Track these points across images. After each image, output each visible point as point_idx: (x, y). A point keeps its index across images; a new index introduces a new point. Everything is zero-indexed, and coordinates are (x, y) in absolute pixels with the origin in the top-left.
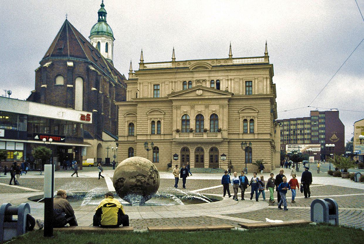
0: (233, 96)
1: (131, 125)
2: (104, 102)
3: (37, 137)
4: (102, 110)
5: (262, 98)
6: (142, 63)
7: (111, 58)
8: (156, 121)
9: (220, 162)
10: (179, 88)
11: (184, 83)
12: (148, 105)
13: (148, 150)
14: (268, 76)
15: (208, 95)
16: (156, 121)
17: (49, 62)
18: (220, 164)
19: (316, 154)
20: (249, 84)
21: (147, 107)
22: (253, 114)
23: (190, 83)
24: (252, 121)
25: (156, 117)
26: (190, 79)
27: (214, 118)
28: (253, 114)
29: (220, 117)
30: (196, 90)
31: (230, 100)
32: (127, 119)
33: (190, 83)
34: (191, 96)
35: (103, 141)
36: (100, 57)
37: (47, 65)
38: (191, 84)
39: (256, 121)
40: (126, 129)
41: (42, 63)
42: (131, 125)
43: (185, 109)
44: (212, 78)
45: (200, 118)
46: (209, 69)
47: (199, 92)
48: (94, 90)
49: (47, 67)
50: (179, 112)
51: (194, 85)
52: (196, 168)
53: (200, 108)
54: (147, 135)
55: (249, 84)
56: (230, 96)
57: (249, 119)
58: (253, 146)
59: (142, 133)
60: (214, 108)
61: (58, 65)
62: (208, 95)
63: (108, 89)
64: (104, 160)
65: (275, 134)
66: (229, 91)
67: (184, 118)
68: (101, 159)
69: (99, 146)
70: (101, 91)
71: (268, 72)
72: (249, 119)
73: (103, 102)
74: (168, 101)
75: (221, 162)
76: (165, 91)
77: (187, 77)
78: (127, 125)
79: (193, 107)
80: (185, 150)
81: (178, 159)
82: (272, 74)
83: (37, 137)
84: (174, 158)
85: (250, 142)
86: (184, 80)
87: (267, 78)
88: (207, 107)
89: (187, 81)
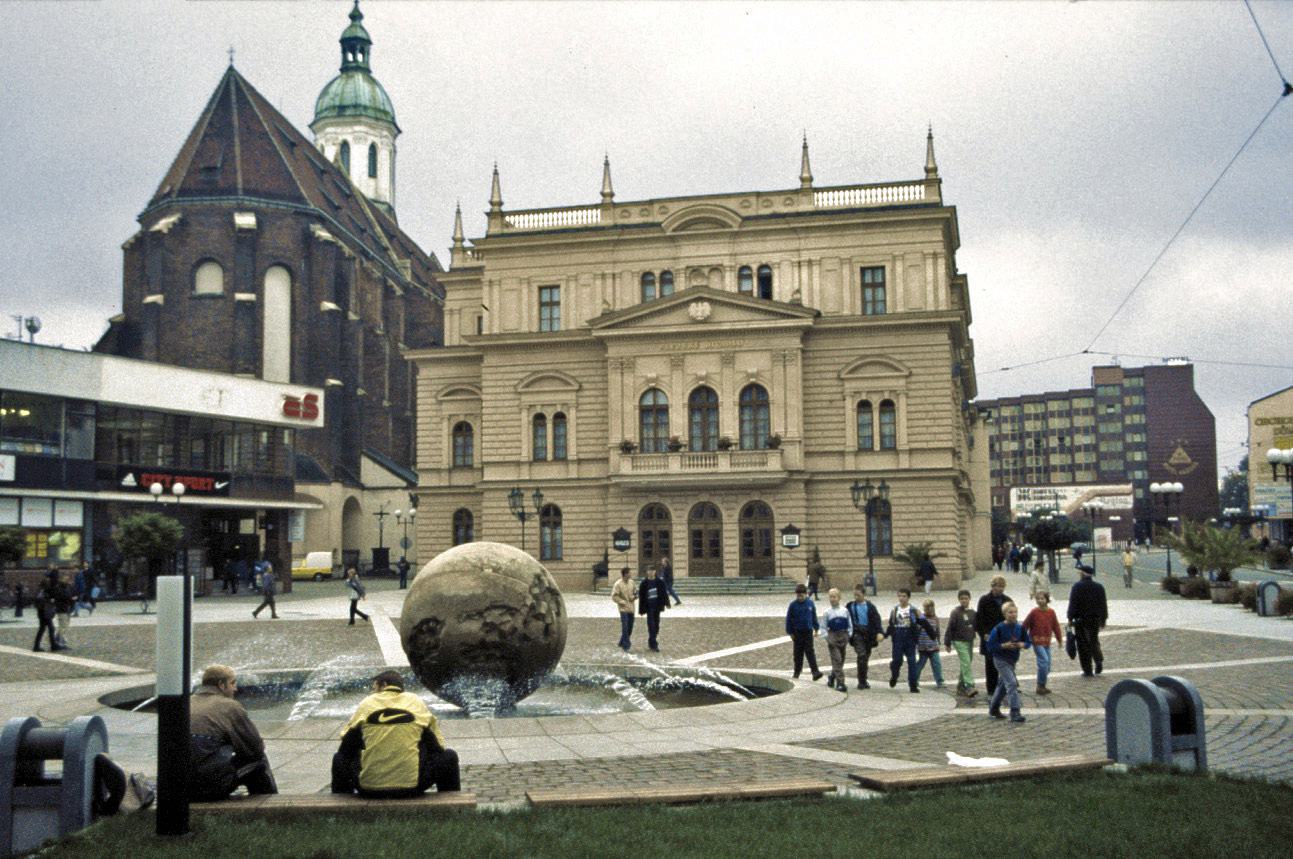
0: (818, 320)
1: (462, 430)
2: (366, 353)
3: (129, 480)
4: (360, 380)
5: (920, 324)
6: (496, 213)
7: (386, 197)
8: (549, 414)
9: (777, 556)
10: (628, 295)
11: (646, 279)
12: (520, 358)
13: (522, 517)
14: (940, 248)
15: (730, 319)
16: (549, 414)
17: (173, 214)
18: (778, 563)
19: (1118, 518)
20: (873, 278)
21: (520, 366)
22: (892, 383)
23: (667, 278)
24: (888, 406)
25: (549, 399)
26: (666, 265)
27: (754, 398)
28: (892, 383)
29: (775, 394)
30: (687, 304)
31: (807, 334)
32: (448, 409)
33: (667, 278)
34: (672, 322)
35: (363, 488)
36: (349, 193)
37: (163, 224)
38: (671, 282)
39: (902, 405)
40: (446, 443)
41: (146, 219)
42: (462, 430)
43: (652, 368)
44: (744, 260)
45: (703, 401)
46: (731, 227)
47: (700, 310)
48: (331, 312)
49: (165, 231)
50: (629, 379)
51: (681, 284)
52: (694, 579)
53: (703, 366)
54: (518, 464)
55: (873, 278)
56: (808, 322)
57: (876, 401)
58: (896, 495)
59: (501, 459)
60: (754, 363)
61: (202, 224)
62: (730, 319)
63: (379, 305)
64: (367, 556)
65: (970, 450)
66: (805, 303)
67: (649, 401)
68: (358, 552)
69: (351, 507)
70: (355, 313)
71: (937, 235)
72: (876, 401)
73: (361, 352)
74: (592, 343)
75: (784, 555)
76: (578, 310)
77: (656, 258)
78: (446, 429)
79: (677, 363)
80: (654, 514)
81: (628, 547)
82: (952, 242)
83: (129, 480)
84: (618, 543)
85: (885, 479)
86: (647, 267)
87: (935, 256)
88: (728, 360)
89: (657, 273)
